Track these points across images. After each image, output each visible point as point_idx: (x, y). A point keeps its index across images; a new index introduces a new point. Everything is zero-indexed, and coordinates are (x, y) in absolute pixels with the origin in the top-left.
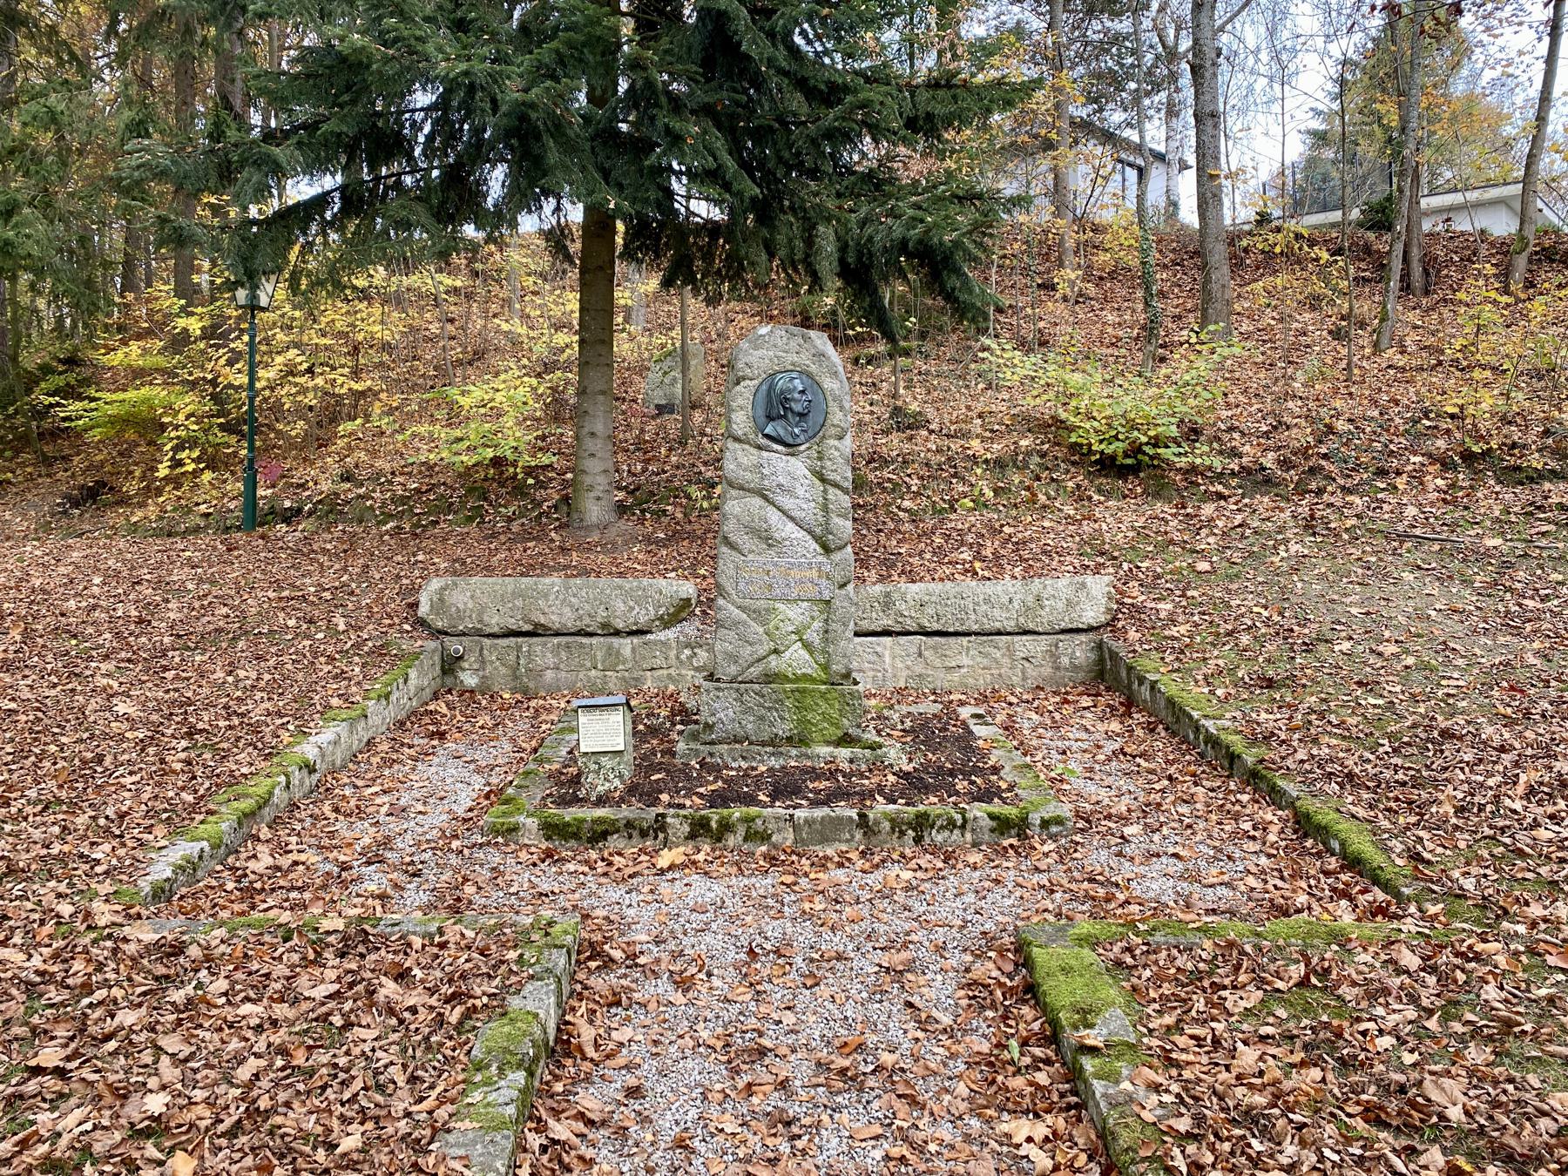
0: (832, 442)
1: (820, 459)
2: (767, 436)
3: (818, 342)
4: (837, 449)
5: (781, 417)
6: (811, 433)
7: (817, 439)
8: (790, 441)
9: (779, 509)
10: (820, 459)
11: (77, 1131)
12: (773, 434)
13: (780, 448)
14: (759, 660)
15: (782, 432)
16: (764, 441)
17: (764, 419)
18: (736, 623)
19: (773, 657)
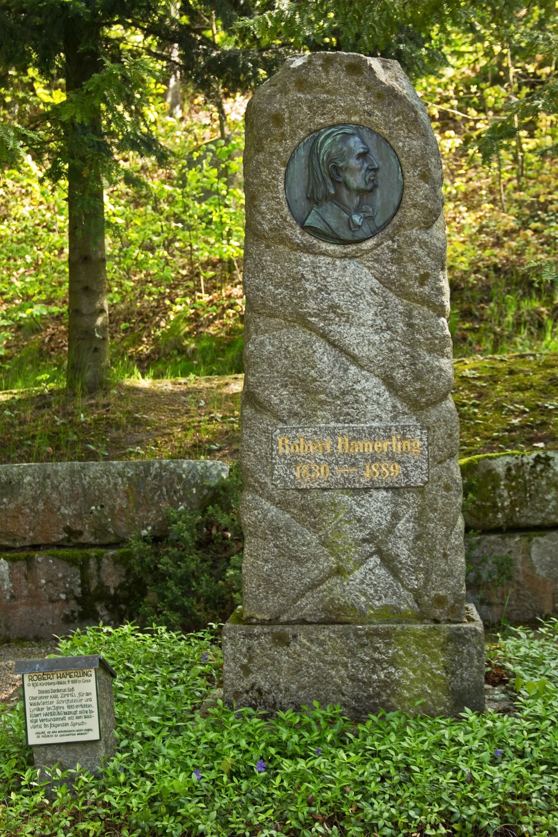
0: (415, 232)
1: (9, 9)
2: (306, 228)
3: (382, 75)
4: (423, 244)
5: (327, 197)
6: (379, 222)
7: (389, 230)
8: (347, 235)
9: (333, 344)
10: (398, 261)
11: (80, 679)
12: (320, 226)
13: (331, 248)
14: (313, 586)
15: (333, 223)
16: (308, 238)
17: (304, 203)
18: (275, 530)
19: (335, 580)
